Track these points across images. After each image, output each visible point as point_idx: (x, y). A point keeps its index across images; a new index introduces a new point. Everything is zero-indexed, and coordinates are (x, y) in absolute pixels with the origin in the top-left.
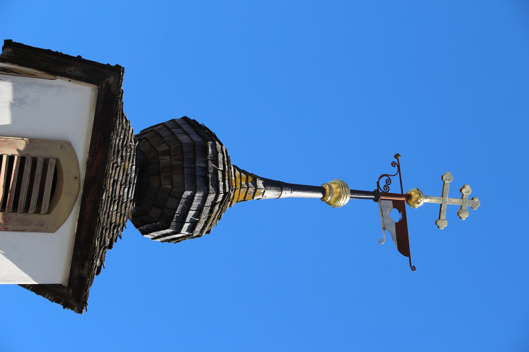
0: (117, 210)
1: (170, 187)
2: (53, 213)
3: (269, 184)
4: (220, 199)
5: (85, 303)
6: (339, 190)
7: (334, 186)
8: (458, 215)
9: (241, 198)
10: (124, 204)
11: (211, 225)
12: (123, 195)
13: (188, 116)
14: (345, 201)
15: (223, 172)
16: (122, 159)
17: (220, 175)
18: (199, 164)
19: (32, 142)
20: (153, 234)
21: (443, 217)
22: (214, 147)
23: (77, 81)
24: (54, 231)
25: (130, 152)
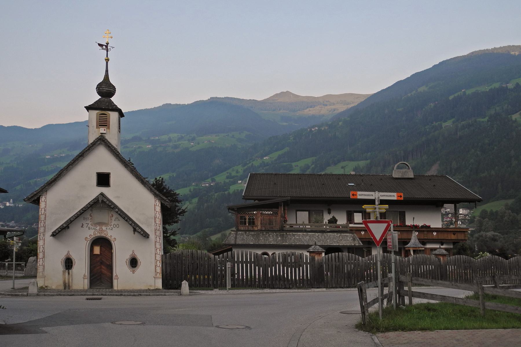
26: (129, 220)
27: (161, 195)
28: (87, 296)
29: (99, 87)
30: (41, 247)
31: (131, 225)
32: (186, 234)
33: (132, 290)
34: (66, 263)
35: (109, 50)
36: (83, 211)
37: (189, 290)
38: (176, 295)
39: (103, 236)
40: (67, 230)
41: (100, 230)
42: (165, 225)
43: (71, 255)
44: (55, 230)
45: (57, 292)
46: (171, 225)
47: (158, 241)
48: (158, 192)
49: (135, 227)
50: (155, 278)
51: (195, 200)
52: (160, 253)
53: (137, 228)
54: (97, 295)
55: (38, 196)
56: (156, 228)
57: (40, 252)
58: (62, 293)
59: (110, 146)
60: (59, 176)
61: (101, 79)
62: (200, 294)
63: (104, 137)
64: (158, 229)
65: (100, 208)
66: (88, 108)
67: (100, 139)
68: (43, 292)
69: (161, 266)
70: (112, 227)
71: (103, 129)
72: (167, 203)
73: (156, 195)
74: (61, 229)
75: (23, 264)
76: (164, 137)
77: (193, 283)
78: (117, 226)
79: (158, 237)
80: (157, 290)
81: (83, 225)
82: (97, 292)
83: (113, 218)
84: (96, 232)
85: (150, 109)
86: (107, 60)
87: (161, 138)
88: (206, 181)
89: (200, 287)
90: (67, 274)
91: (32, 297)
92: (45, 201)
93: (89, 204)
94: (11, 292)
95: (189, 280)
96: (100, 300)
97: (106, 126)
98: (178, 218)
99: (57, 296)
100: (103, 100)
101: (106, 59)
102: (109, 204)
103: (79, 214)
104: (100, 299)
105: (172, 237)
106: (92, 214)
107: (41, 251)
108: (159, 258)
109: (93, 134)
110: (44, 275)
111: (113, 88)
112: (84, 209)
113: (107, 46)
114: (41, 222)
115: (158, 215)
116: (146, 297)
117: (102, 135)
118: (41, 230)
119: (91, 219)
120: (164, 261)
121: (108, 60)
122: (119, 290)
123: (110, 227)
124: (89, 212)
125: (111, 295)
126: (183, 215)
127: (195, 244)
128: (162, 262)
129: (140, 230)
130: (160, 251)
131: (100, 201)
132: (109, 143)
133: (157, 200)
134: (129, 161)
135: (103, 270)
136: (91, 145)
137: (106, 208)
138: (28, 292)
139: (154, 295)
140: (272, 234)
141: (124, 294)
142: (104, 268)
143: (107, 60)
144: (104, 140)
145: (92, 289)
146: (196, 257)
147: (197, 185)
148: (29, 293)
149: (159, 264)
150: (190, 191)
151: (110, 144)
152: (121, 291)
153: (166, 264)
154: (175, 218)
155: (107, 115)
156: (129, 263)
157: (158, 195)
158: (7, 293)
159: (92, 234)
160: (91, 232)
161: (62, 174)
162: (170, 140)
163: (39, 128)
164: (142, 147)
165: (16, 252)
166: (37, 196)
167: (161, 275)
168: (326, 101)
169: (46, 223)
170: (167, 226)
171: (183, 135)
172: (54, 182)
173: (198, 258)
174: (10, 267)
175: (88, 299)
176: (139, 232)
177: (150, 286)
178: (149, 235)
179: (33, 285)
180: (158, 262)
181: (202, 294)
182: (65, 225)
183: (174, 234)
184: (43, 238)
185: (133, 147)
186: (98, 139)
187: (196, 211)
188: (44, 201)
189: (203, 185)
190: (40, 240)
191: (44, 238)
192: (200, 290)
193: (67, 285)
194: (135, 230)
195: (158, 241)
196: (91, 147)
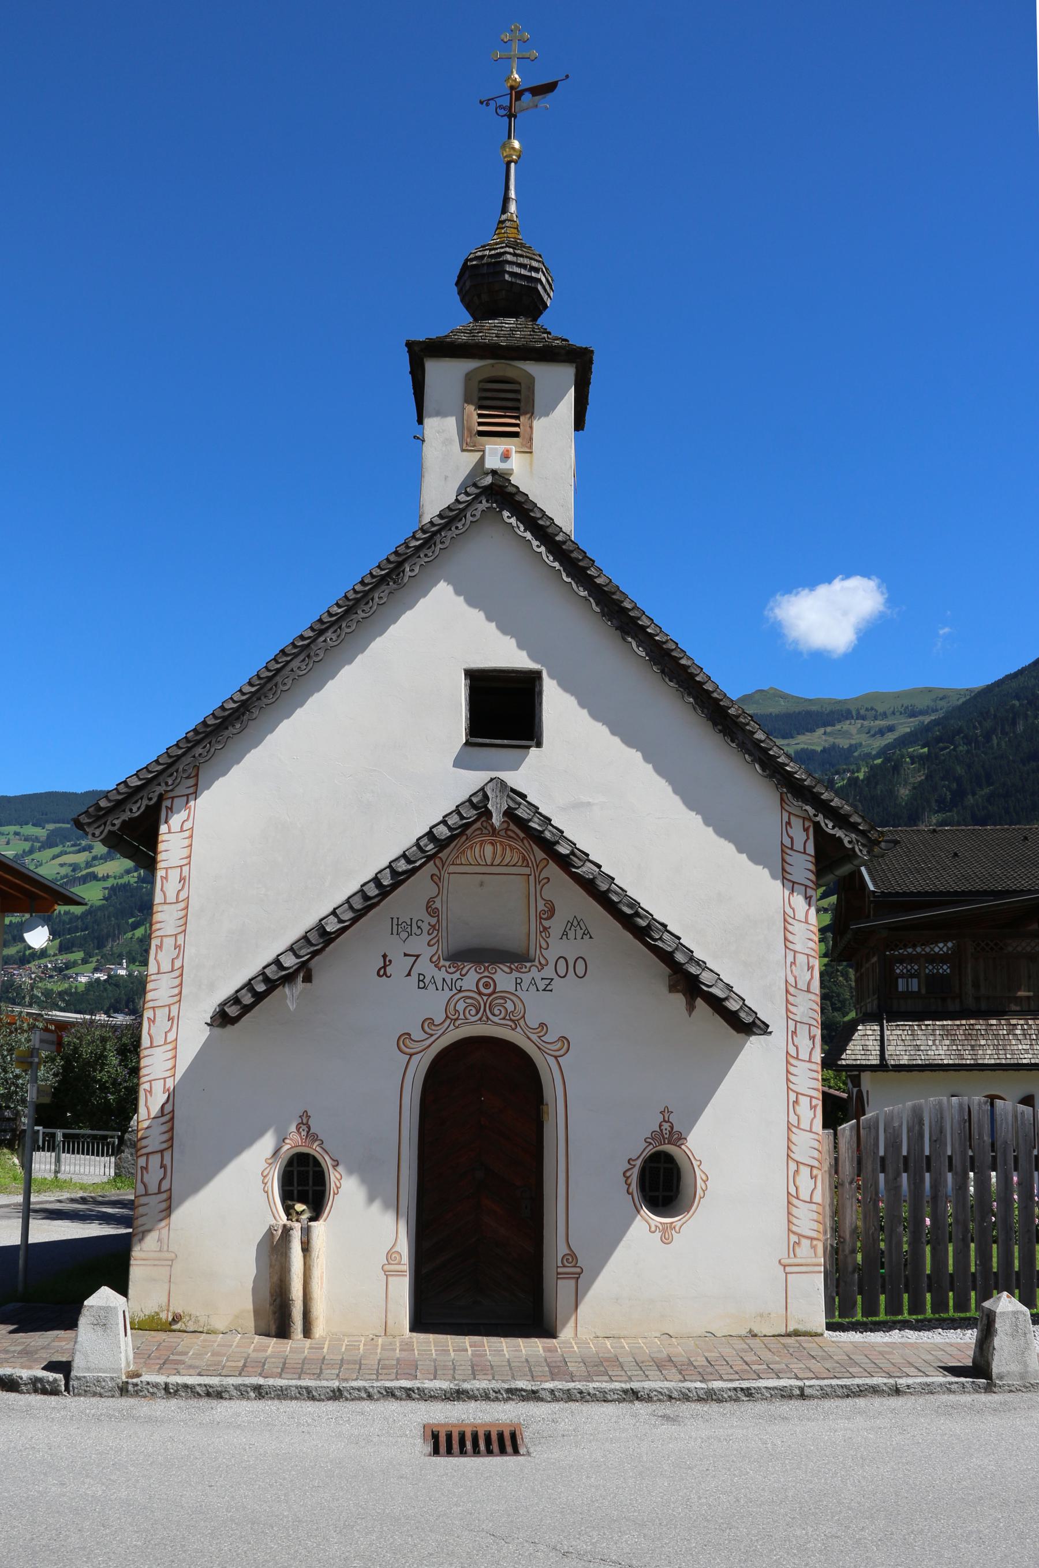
0: (520, 331)
1: (504, 292)
2: (520, 381)
3: (505, 209)
4: (511, 250)
5: (586, 348)
6: (507, 150)
7: (505, 154)
8: (525, 42)
9: (516, 231)
10: (518, 326)
11: (534, 254)
12: (510, 328)
13: (455, 282)
14: (516, 144)
15: (490, 250)
16: (480, 332)
17: (493, 252)
18: (485, 270)
19: (467, 400)
20: (545, 299)
21: (527, 55)
22: (472, 260)
23: (550, 363)
24: (534, 378)
25: (477, 326)
41: (480, 993)
44: (237, 991)
50: (788, 1269)
55: (150, 799)
56: (791, 980)
64: (802, 984)
70: (549, 972)
75: (112, 1137)
97: (516, 435)
106: (438, 900)
114: (160, 947)
119: (433, 927)
140: (1022, 1025)
166: (145, 802)
168: (867, 709)
169: (190, 951)
172: (238, 718)
177: (761, 1316)
182: (290, 961)
191: (171, 1037)
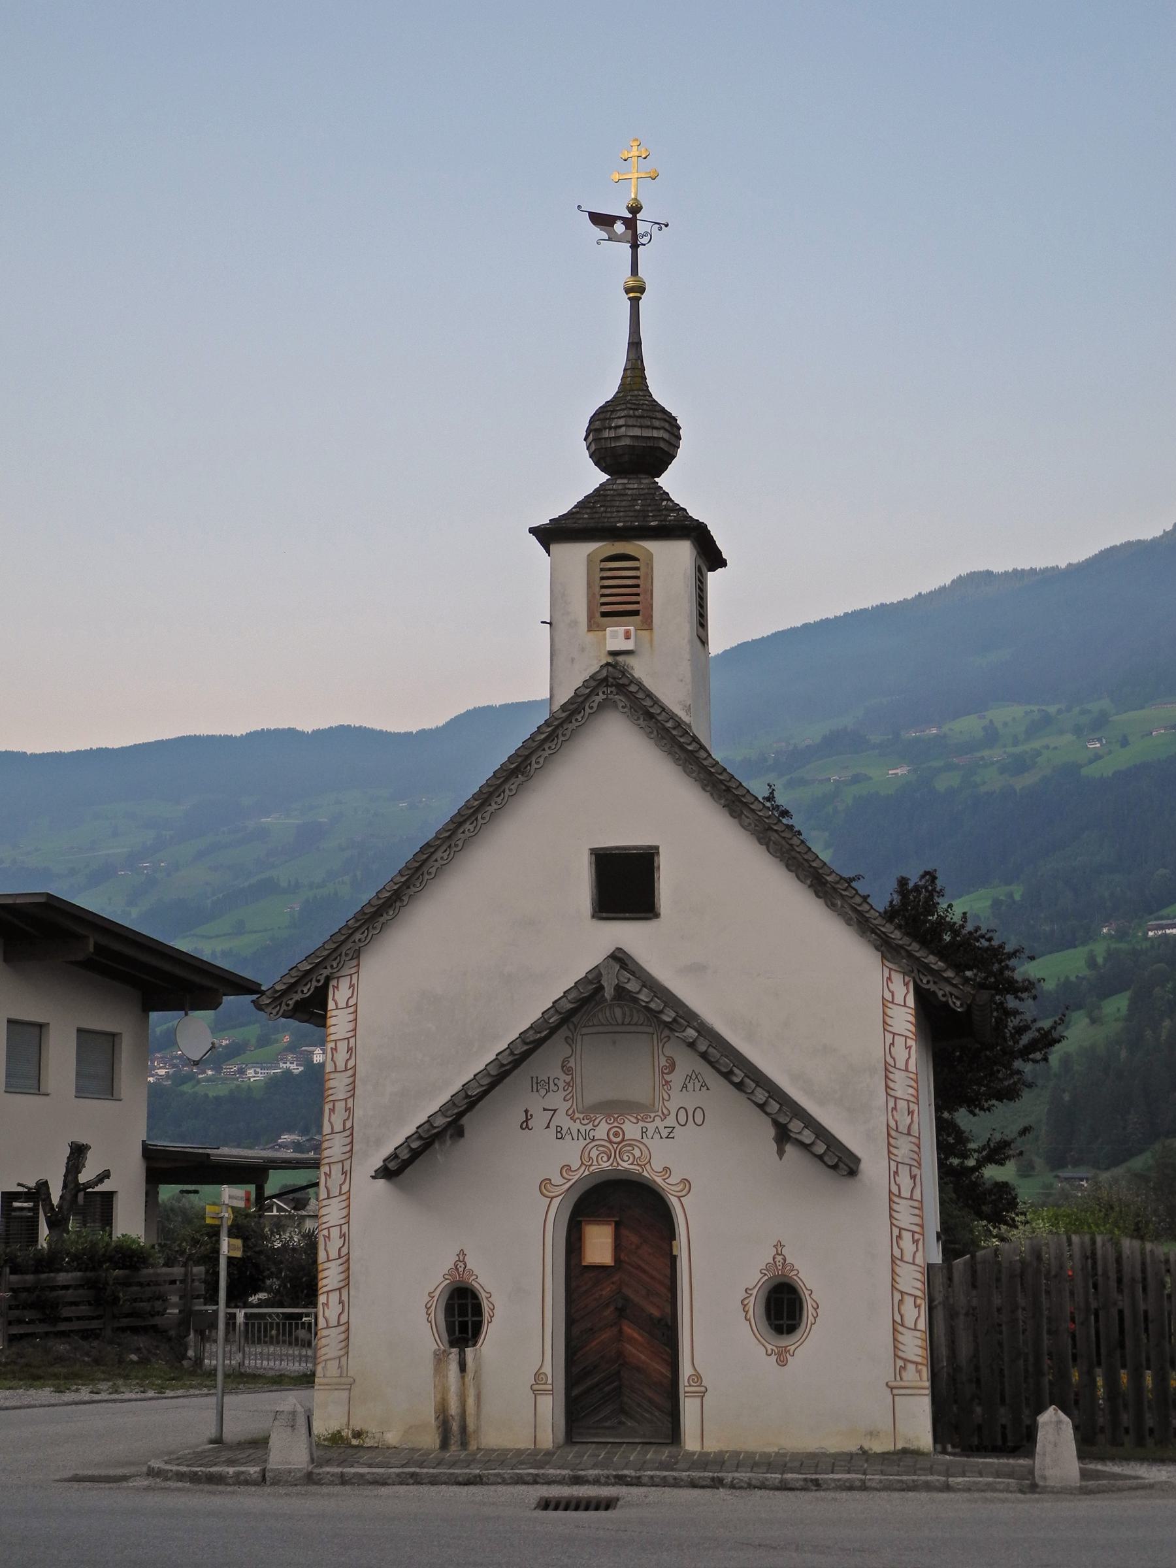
26: (753, 1085)
27: (915, 946)
28: (545, 1487)
29: (598, 424)
30: (335, 1232)
31: (762, 1107)
32: (1077, 1163)
33: (777, 1454)
34: (449, 1310)
35: (641, 241)
36: (527, 1044)
37: (1081, 1456)
38: (1007, 1490)
39: (626, 1171)
40: (449, 1142)
41: (611, 1142)
42: (952, 1110)
43: (471, 1272)
45: (402, 1466)
46: (982, 1109)
47: (906, 1193)
48: (897, 935)
49: (783, 1120)
50: (896, 1391)
51: (1118, 1005)
52: (919, 1255)
53: (795, 1126)
54: (596, 1482)
55: (318, 981)
56: (892, 1124)
57: (328, 1260)
58: (425, 1470)
59: (652, 710)
60: (413, 875)
61: (609, 389)
62: (1143, 1487)
63: (624, 672)
64: (903, 1128)
65: (610, 1029)
66: (548, 535)
67: (606, 679)
68: (338, 1466)
69: (922, 1324)
70: (671, 1121)
71: (621, 630)
72: (948, 989)
73: (887, 949)
74: (420, 1138)
76: (968, 726)
77: (1101, 1421)
78: (695, 1117)
79: (904, 1172)
80: (906, 1456)
81: (528, 1116)
82: (594, 1467)
83: (677, 1078)
84: (594, 1154)
85: (899, 602)
86: (636, 291)
87: (951, 729)
88: (1164, 912)
89: (1140, 1442)
90: (454, 1367)
91: (282, 1490)
92: (352, 1002)
93: (557, 1011)
94: (198, 1457)
95: (1076, 1402)
96: (607, 1509)
97: (635, 613)
98: (1019, 1072)
99: (401, 1484)
100: (620, 487)
101: (631, 284)
102: (652, 1006)
103: (505, 1062)
104: (608, 1504)
105: (991, 1172)
106: (572, 1060)
107: (333, 1254)
108: (912, 1281)
109: (573, 660)
110: (347, 1376)
111: (667, 426)
112: (532, 1036)
113: (631, 224)
114: (332, 1110)
115: (900, 1053)
116: (844, 1495)
117: (617, 663)
118: (334, 1149)
119: (568, 1084)
120: (939, 1298)
121: (642, 290)
122: (708, 1454)
123: (661, 1125)
124: (557, 1049)
125: (665, 1483)
126: (1046, 1059)
127: (1117, 1209)
128: (931, 1301)
129: (807, 1137)
130: (915, 1242)
131: (609, 993)
132: (649, 695)
133: (895, 976)
134: (770, 798)
135: (628, 1346)
136: (564, 715)
137: (640, 1029)
138: (266, 1461)
139: (888, 1487)
141: (728, 1477)
142: (636, 1335)
143: (636, 291)
144: (624, 685)
145: (576, 1449)
146: (1113, 1275)
147: (1121, 935)
148: (269, 1467)
149: (915, 1315)
150: (1092, 963)
151: (656, 702)
152: (718, 1461)
153: (952, 1314)
154: (1000, 1075)
155: (636, 559)
156: (761, 1310)
157: (901, 947)
158: (175, 1468)
159: (575, 1165)
160: (571, 1152)
161: (425, 869)
162: (991, 737)
163: (437, 728)
164: (870, 778)
165: (230, 1260)
166: (314, 984)
167: (926, 1373)
169: (358, 1113)
170: (962, 1118)
171: (1052, 709)
172: (391, 906)
173: (1126, 1280)
174: (265, 1331)
175: (545, 1504)
176: (806, 1147)
177: (871, 1434)
178: (857, 1160)
179: (289, 1429)
180: (909, 1301)
181: (1151, 1486)
182: (440, 1121)
183: (996, 1153)
184: (341, 1185)
185: (830, 779)
186: (593, 684)
187: (1124, 1054)
188: (347, 1007)
189: (1151, 934)
190: (329, 1198)
192: (1142, 1459)
193: (455, 1426)
194: (783, 1136)
195: (906, 1193)
196: (561, 725)
